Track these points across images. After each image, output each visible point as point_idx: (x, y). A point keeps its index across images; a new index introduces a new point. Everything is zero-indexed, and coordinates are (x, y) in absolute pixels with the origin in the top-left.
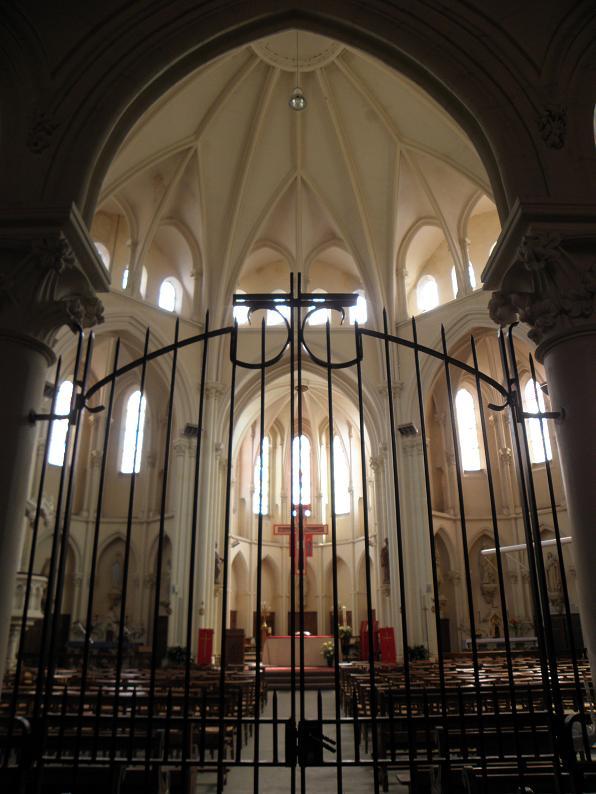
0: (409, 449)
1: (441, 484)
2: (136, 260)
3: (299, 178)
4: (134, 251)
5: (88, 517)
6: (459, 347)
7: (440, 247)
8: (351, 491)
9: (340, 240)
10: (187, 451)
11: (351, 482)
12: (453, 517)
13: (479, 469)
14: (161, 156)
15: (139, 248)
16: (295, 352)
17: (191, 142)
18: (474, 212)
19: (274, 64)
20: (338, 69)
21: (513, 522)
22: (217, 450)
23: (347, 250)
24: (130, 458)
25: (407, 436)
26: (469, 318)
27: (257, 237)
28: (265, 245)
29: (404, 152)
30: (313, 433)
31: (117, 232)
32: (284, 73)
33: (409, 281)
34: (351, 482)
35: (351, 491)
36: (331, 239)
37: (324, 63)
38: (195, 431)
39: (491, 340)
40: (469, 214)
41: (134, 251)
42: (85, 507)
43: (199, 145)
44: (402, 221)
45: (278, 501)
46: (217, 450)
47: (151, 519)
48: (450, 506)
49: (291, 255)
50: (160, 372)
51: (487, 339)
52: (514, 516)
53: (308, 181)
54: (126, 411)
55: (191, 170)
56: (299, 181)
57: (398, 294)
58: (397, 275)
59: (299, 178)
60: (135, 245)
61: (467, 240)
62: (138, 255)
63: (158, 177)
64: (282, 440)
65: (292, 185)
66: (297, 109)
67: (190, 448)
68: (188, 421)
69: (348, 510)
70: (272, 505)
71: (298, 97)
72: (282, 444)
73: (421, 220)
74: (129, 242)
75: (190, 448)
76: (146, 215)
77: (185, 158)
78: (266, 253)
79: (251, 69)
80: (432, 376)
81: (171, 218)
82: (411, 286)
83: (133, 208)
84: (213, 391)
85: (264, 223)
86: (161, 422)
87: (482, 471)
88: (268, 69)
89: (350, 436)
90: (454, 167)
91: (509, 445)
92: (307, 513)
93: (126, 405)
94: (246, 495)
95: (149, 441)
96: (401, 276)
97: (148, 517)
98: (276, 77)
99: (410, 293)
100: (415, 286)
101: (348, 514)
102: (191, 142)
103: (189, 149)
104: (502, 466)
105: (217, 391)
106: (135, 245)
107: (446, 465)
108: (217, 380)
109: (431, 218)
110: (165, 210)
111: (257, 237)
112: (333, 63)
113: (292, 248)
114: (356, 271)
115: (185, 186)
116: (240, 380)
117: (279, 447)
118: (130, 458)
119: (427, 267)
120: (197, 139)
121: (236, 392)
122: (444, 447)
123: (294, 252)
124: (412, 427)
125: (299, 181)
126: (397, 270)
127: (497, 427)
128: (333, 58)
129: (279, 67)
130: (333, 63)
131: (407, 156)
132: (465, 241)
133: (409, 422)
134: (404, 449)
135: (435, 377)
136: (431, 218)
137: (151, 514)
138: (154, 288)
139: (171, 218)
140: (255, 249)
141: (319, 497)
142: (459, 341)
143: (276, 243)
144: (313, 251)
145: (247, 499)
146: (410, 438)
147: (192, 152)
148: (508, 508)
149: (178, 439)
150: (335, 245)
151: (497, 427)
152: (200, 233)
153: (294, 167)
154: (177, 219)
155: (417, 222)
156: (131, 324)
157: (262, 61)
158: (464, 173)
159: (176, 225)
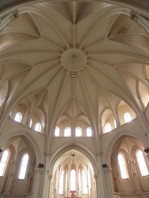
0: (106, 172)
1: (116, 183)
2: (29, 116)
3: (74, 97)
4: (29, 114)
5: (5, 194)
6: (117, 143)
7: (111, 115)
8: (88, 187)
9: (84, 114)
10: (39, 172)
11: (88, 184)
12: (121, 194)
13: (126, 178)
14: (37, 91)
15: (30, 113)
16: (73, 144)
17: (46, 87)
18: (119, 106)
19: (68, 69)
20: (83, 71)
21: (140, 196)
22: (48, 172)
23: (86, 117)
24: (22, 175)
25: (105, 168)
26: (120, 133)
27: (62, 113)
28: (64, 115)
29: (100, 90)
30: (77, 170)
31: (25, 110)
32: (70, 71)
33: (103, 124)
34: (88, 184)
35: (88, 187)
36: (82, 113)
37: (80, 69)
38: (41, 166)
39: (127, 139)
40: (118, 106)
41: (29, 114)
42: (5, 191)
43: (48, 88)
44: (100, 109)
45: (66, 190)
46: (48, 172)
47: (25, 195)
48: (119, 190)
49: (70, 117)
50: (32, 147)
51: (126, 139)
52: (140, 194)
53: (76, 98)
54: (23, 160)
55: (46, 94)
56: (73, 98)
57: (100, 127)
58: (100, 122)
59: (74, 97)
60: (29, 113)
61: (118, 112)
62: (30, 115)
63: (37, 96)
64: (68, 171)
65: (72, 99)
66: (73, 77)
67: (40, 171)
68: (40, 163)
69: (87, 193)
70: (64, 192)
71: (74, 74)
72: (68, 172)
73: (105, 108)
74: (28, 112)
75: (40, 171)
76: (33, 106)
77: (44, 91)
78: (65, 117)
79: (62, 70)
80: (113, 146)
81: (39, 107)
82: (104, 125)
83: (30, 104)
84: (48, 154)
85: (64, 109)
86: (32, 163)
87: (127, 179)
88: (66, 70)
89: (87, 170)
90: (114, 94)
91: (135, 170)
92: (75, 194)
93: (23, 158)
94: (56, 188)
95: (28, 169)
96: (101, 123)
97: (25, 194)
98: (68, 72)
99: (103, 127)
100: (104, 126)
101: (87, 194)
102: (46, 87)
103: (45, 89)
104: (134, 177)
105: (49, 154)
106: (29, 113)
107: (117, 177)
108: (49, 151)
109: (108, 107)
110: (38, 104)
111: (62, 113)
112: (82, 69)
113: (71, 115)
114: (89, 122)
115: (44, 99)
116: (41, 3)
117: (67, 173)
118: (22, 175)
119: (107, 121)
120: (48, 87)
121: (39, 4)
122: (116, 172)
123: (72, 117)
124: (106, 165)
125: (73, 98)
126: (99, 121)
127: (131, 165)
128: (82, 68)
129: (69, 70)
130: (82, 69)
131: (101, 91)
132: (117, 113)
133: (105, 163)
134: (104, 172)
135: (112, 150)
136: (108, 107)
137: (26, 193)
138: (34, 125)
139: (39, 107)
140: (61, 117)
141: (78, 189)
142: (119, 139)
143: (67, 115)
144: (77, 117)
145: (57, 189)
146: (106, 168)
147: (46, 89)
148: (138, 191)
149: (37, 169)
150: (83, 115)
151: (131, 165)
152: (47, 111)
153: (72, 95)
154: (41, 107)
155: (104, 109)
156: (26, 133)
157: (65, 69)
158: (116, 95)
159: (41, 109)
